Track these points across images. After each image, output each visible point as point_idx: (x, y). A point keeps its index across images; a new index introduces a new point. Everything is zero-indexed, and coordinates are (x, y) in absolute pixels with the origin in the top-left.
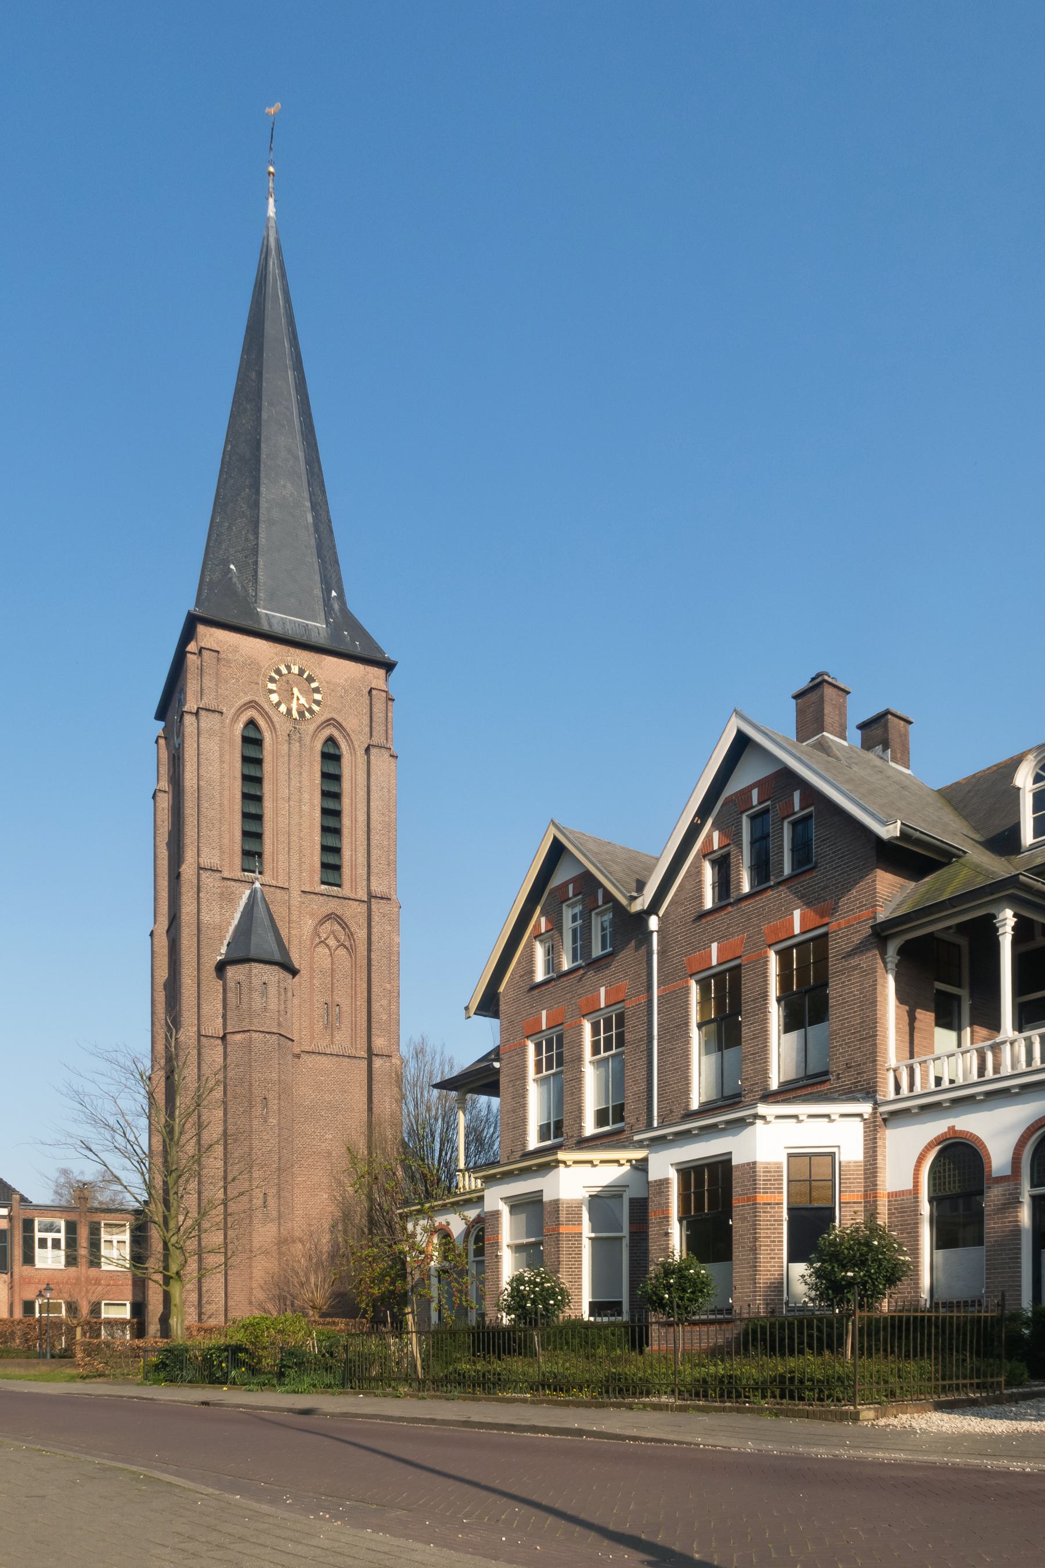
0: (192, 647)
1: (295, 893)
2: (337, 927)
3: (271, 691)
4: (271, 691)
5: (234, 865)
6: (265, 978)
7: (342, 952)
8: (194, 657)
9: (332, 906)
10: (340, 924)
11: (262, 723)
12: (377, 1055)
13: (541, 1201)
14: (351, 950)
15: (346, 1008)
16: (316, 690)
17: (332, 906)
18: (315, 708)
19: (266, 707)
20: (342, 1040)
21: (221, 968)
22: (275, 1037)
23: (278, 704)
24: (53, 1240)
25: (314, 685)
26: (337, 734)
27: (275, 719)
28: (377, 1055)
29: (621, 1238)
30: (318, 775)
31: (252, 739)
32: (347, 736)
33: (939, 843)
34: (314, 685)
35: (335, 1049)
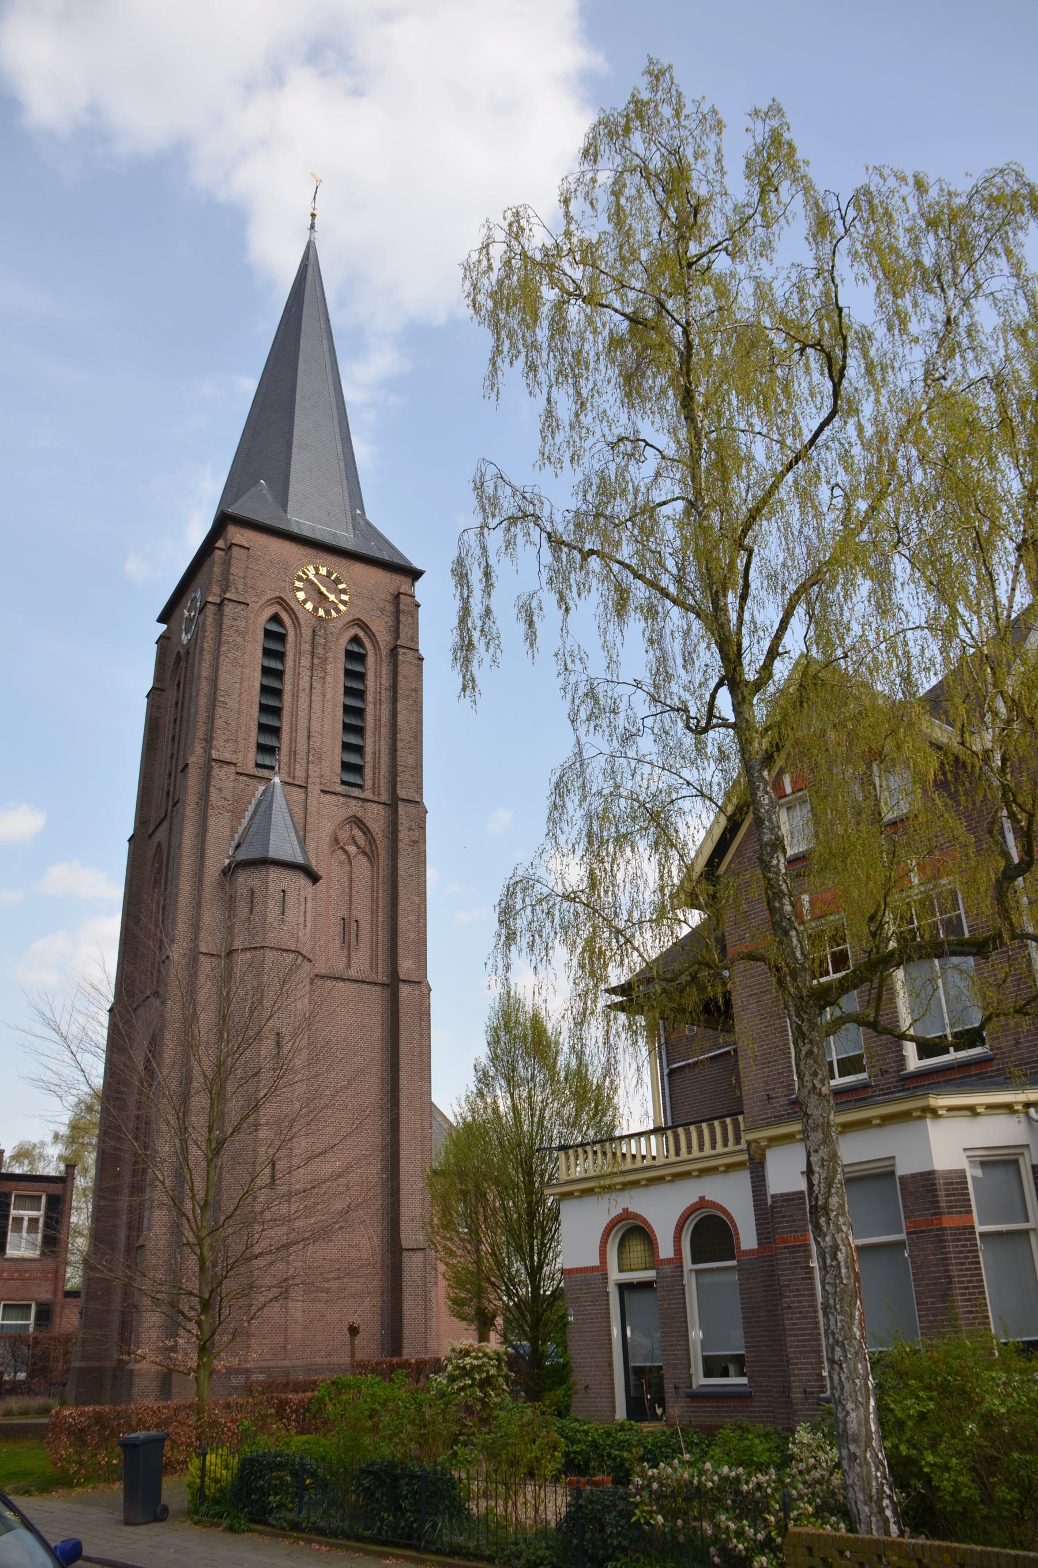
0: (220, 543)
1: (314, 790)
2: (357, 832)
3: (299, 589)
4: (299, 589)
5: (249, 758)
6: (284, 885)
7: (362, 860)
8: (221, 553)
9: (354, 808)
10: (360, 828)
11: (284, 616)
12: (404, 981)
13: (892, 1173)
14: (371, 856)
15: (365, 925)
16: (344, 591)
17: (354, 808)
18: (342, 607)
19: (293, 604)
20: (361, 964)
21: (229, 872)
22: (292, 956)
23: (305, 601)
24: (30, 1220)
25: (341, 587)
26: (361, 634)
27: (300, 616)
28: (404, 981)
29: (1027, 1220)
30: (342, 673)
31: (275, 637)
32: (371, 636)
33: (203, 715)
34: (341, 587)
35: (353, 973)
